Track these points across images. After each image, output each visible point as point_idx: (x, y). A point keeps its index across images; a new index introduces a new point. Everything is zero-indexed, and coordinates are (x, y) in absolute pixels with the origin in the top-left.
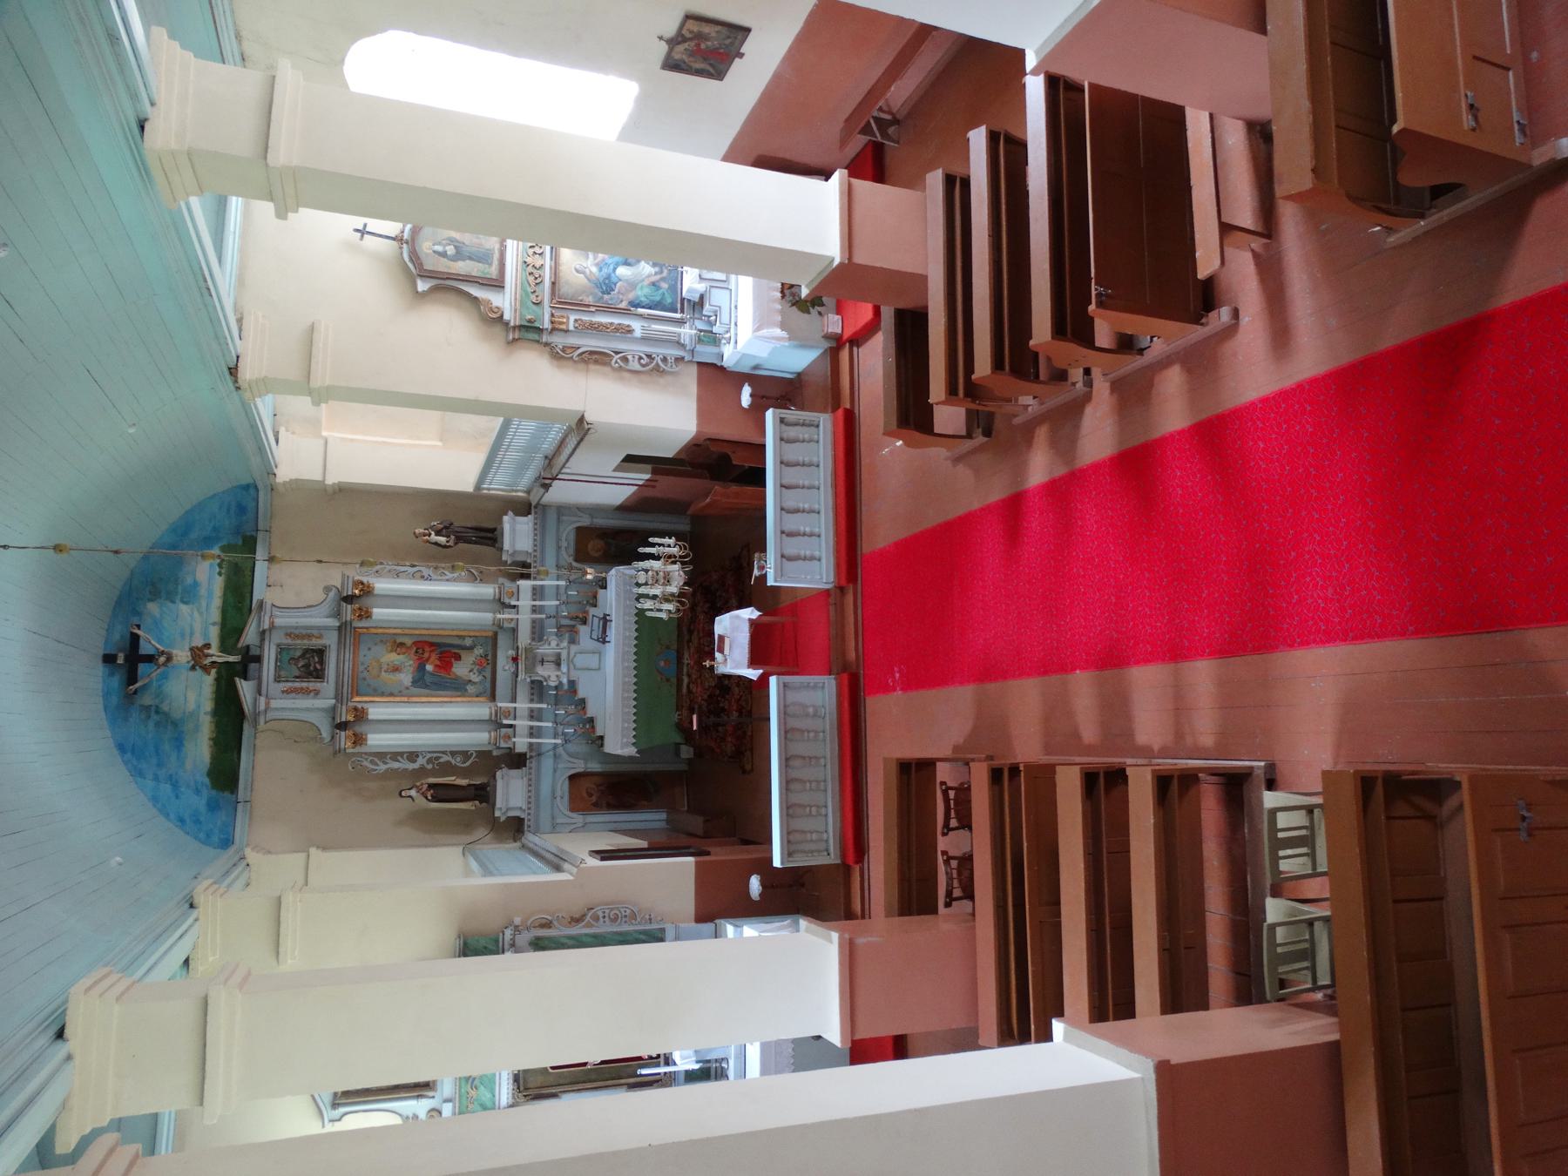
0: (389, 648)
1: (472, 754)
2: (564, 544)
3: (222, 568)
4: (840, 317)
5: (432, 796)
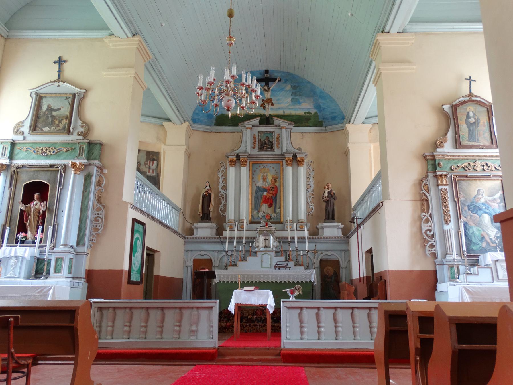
0: (273, 176)
1: (225, 214)
2: (329, 253)
3: (308, 114)
5: (206, 195)
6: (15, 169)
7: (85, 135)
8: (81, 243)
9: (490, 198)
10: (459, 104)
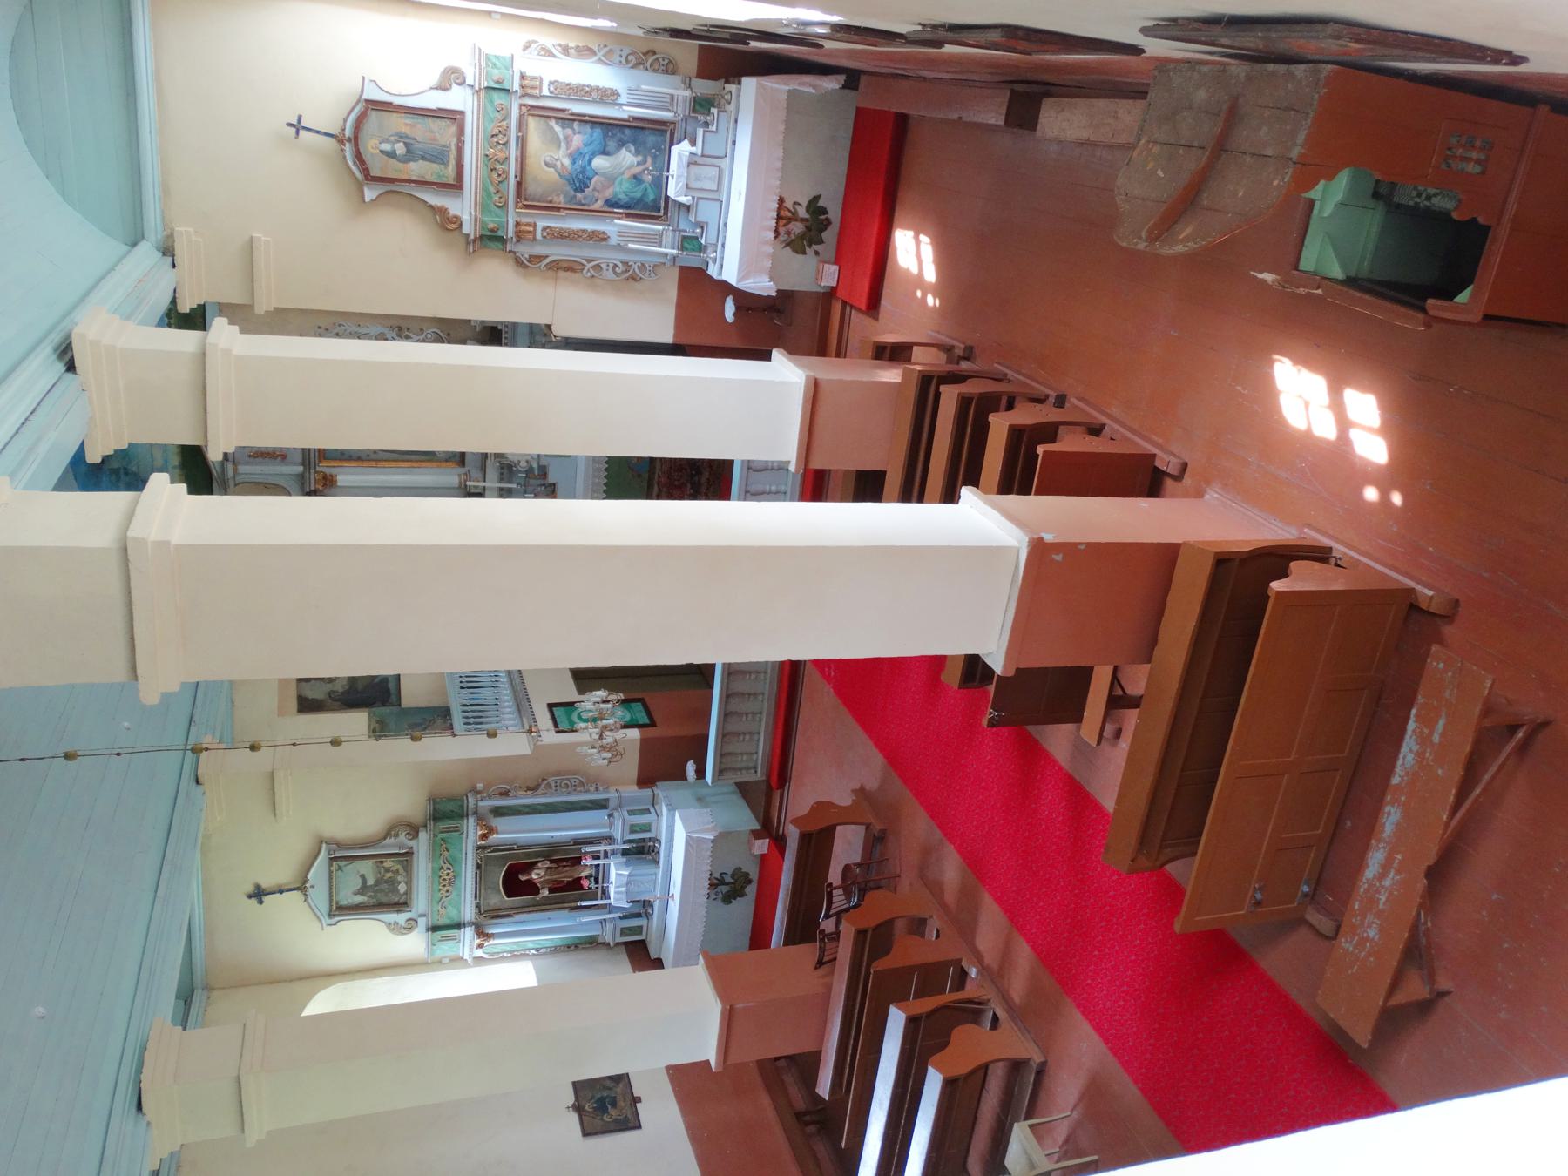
3: (171, 318)
4: (836, 267)
6: (482, 917)
7: (414, 831)
8: (604, 803)
9: (563, 145)
10: (364, 170)
